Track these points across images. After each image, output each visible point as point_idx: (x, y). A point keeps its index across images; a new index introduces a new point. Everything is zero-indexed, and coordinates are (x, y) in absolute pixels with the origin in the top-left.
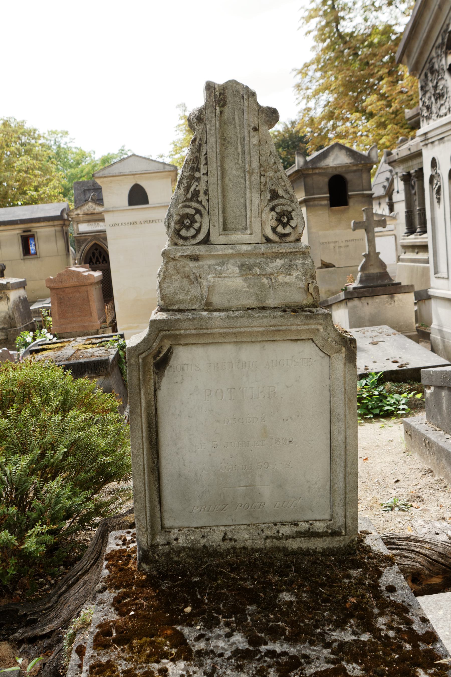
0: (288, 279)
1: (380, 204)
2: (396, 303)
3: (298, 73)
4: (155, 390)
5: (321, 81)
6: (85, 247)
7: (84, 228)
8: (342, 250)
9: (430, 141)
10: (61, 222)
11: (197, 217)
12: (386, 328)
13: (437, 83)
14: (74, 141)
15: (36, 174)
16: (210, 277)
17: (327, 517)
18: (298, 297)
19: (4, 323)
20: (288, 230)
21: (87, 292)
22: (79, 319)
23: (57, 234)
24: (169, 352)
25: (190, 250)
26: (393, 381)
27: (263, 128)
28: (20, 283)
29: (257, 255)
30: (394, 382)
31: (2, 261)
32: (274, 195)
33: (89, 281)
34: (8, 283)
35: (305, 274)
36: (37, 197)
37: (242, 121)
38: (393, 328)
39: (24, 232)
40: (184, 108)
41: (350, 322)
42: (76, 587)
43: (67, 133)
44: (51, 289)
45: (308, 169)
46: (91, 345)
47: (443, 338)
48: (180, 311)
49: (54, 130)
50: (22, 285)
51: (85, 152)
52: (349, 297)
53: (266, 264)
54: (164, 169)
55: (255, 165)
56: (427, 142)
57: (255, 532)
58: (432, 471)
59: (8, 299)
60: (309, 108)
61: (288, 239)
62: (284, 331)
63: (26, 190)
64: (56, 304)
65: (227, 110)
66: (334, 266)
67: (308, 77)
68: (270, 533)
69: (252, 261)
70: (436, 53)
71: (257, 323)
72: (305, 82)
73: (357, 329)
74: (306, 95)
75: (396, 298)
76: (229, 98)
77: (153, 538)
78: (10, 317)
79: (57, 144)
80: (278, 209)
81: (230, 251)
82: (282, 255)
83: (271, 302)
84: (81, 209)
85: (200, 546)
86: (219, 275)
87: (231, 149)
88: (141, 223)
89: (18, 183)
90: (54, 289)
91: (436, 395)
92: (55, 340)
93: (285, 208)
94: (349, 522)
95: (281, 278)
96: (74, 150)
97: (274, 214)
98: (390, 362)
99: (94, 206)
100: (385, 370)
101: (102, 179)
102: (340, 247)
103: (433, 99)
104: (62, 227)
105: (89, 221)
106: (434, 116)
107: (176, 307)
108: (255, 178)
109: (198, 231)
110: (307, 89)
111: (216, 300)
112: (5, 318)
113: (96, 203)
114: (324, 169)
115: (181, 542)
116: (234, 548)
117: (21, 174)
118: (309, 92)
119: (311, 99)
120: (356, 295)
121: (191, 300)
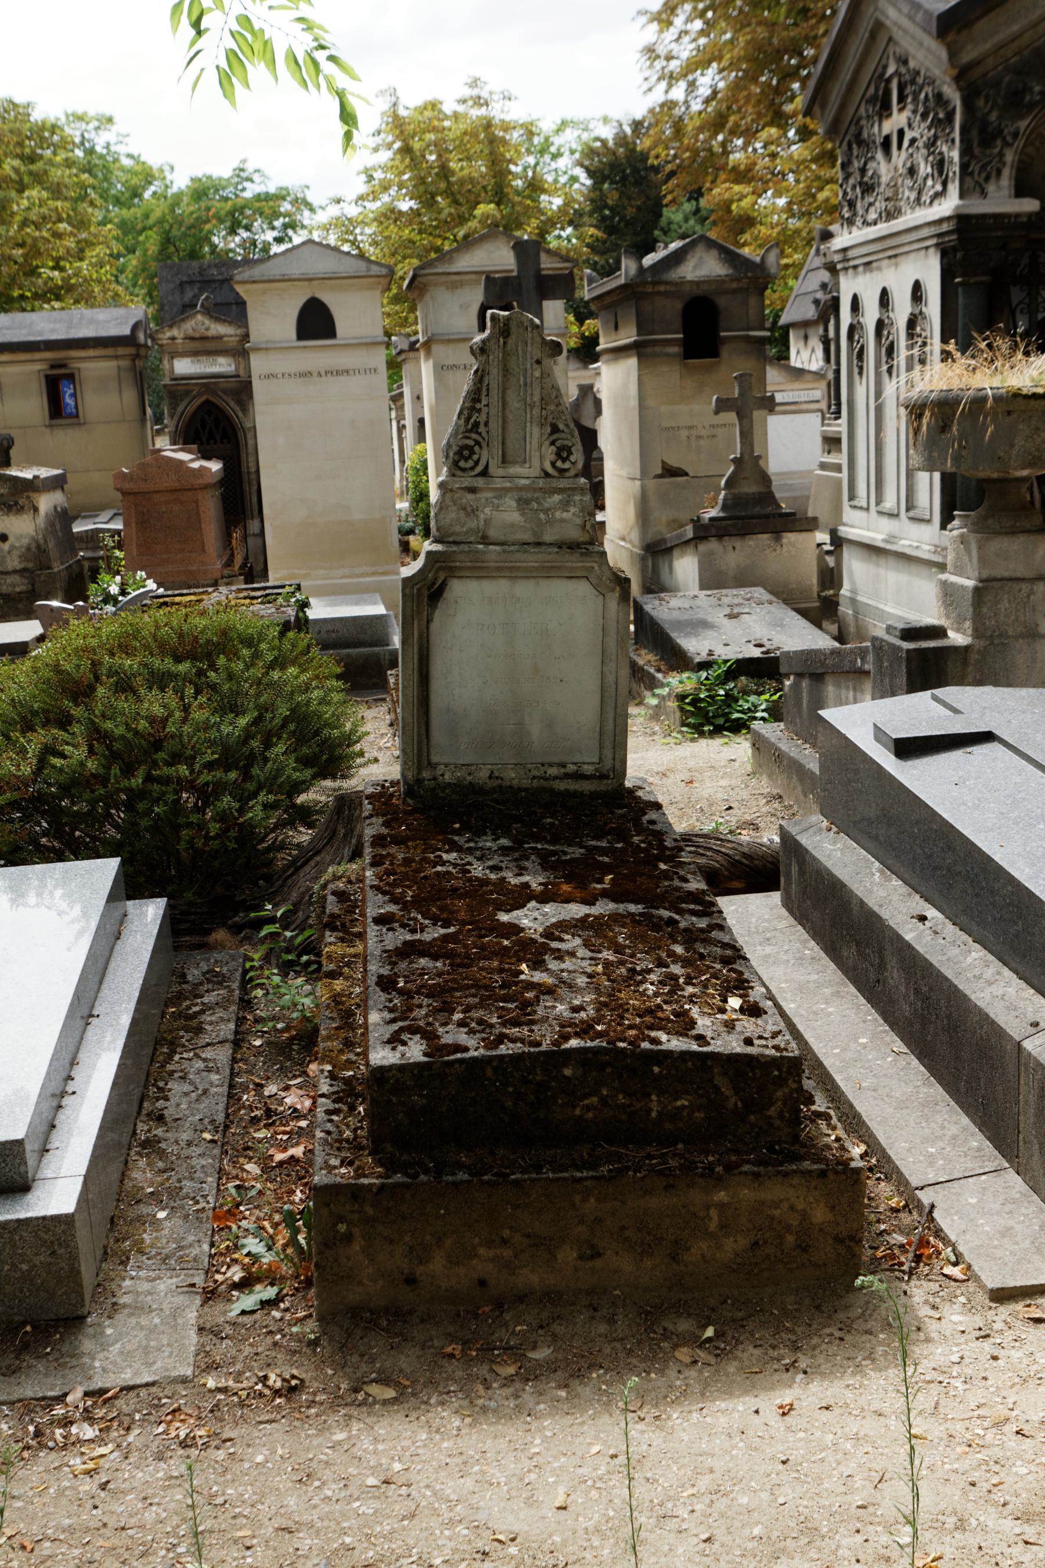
0: (565, 515)
1: (806, 338)
2: (785, 549)
3: (652, 21)
4: (428, 622)
5: (702, 41)
6: (188, 407)
7: (184, 366)
8: (703, 443)
9: (852, 263)
10: (131, 350)
11: (476, 448)
12: (759, 592)
13: (865, 164)
14: (127, 140)
15: (61, 230)
16: (487, 510)
17: (596, 760)
18: (574, 534)
19: (27, 560)
20: (567, 465)
21: (197, 502)
22: (179, 556)
23: (122, 374)
24: (444, 584)
25: (468, 482)
26: (750, 675)
27: (547, 362)
28: (57, 476)
29: (535, 490)
30: (753, 677)
31: (6, 428)
32: (555, 429)
33: (201, 481)
34: (36, 477)
35: (582, 510)
36: (60, 283)
37: (525, 353)
38: (772, 592)
39: (53, 367)
40: (394, 99)
41: (701, 580)
42: (307, 869)
43: (110, 120)
44: (125, 493)
45: (644, 283)
46: (248, 601)
47: (856, 612)
48: (455, 543)
49: (80, 111)
50: (58, 483)
51: (151, 168)
52: (702, 534)
53: (544, 499)
54: (368, 270)
55: (536, 398)
56: (846, 265)
57: (522, 772)
58: (780, 797)
59: (36, 510)
60: (672, 102)
61: (567, 474)
62: (559, 568)
63: (37, 267)
64: (133, 525)
65: (511, 341)
66: (687, 474)
67: (672, 29)
68: (537, 773)
69: (529, 495)
70: (867, 111)
71: (532, 559)
72: (667, 41)
73: (709, 592)
74: (666, 70)
75: (784, 541)
76: (514, 330)
77: (419, 772)
78: (38, 547)
79: (87, 145)
80: (558, 444)
81: (508, 485)
82: (561, 491)
83: (548, 538)
84: (179, 328)
85: (466, 783)
86: (496, 508)
87: (513, 381)
88: (320, 375)
89: (20, 251)
90: (130, 494)
91: (795, 686)
92: (161, 591)
93: (565, 442)
94: (618, 765)
95: (558, 514)
96: (126, 162)
97: (553, 448)
98: (751, 646)
99: (207, 322)
100: (740, 656)
101: (248, 286)
102: (699, 437)
103: (858, 189)
104: (134, 360)
105: (195, 354)
106: (859, 221)
107: (451, 539)
108: (536, 411)
109: (477, 463)
110: (669, 58)
111: (493, 533)
112: (28, 549)
113: (211, 317)
114: (677, 284)
115: (447, 777)
116: (500, 786)
117: (28, 230)
118: (674, 65)
119: (677, 80)
120: (713, 532)
121: (467, 533)
